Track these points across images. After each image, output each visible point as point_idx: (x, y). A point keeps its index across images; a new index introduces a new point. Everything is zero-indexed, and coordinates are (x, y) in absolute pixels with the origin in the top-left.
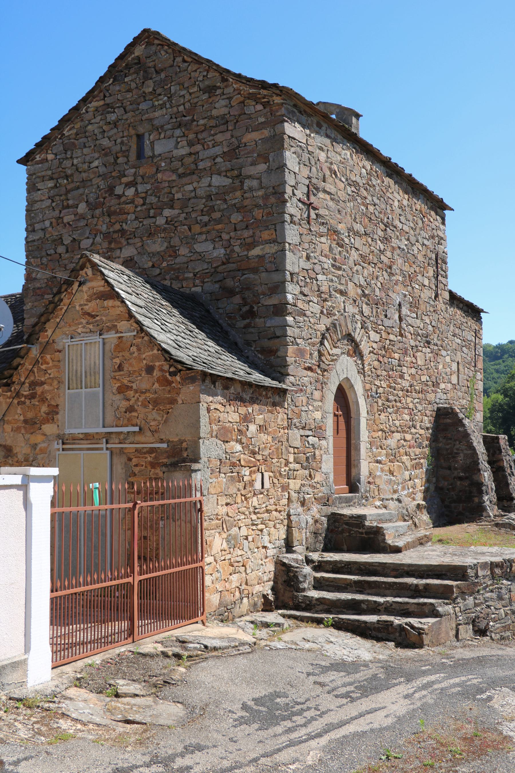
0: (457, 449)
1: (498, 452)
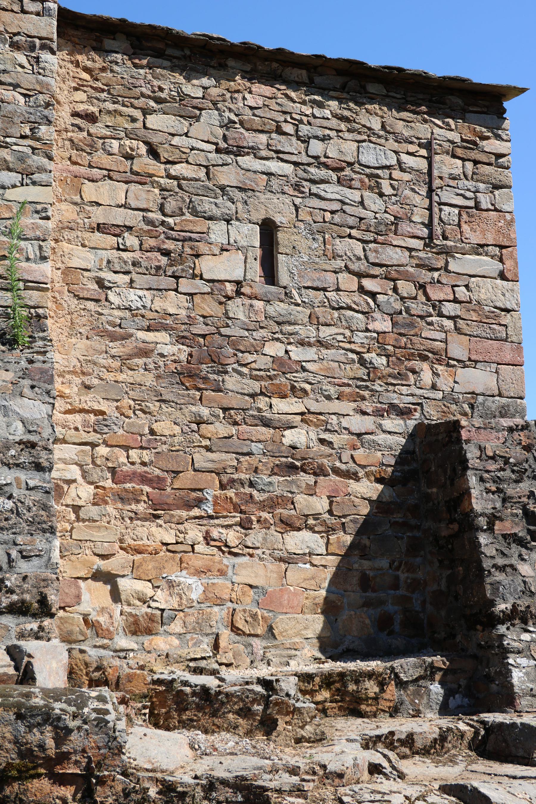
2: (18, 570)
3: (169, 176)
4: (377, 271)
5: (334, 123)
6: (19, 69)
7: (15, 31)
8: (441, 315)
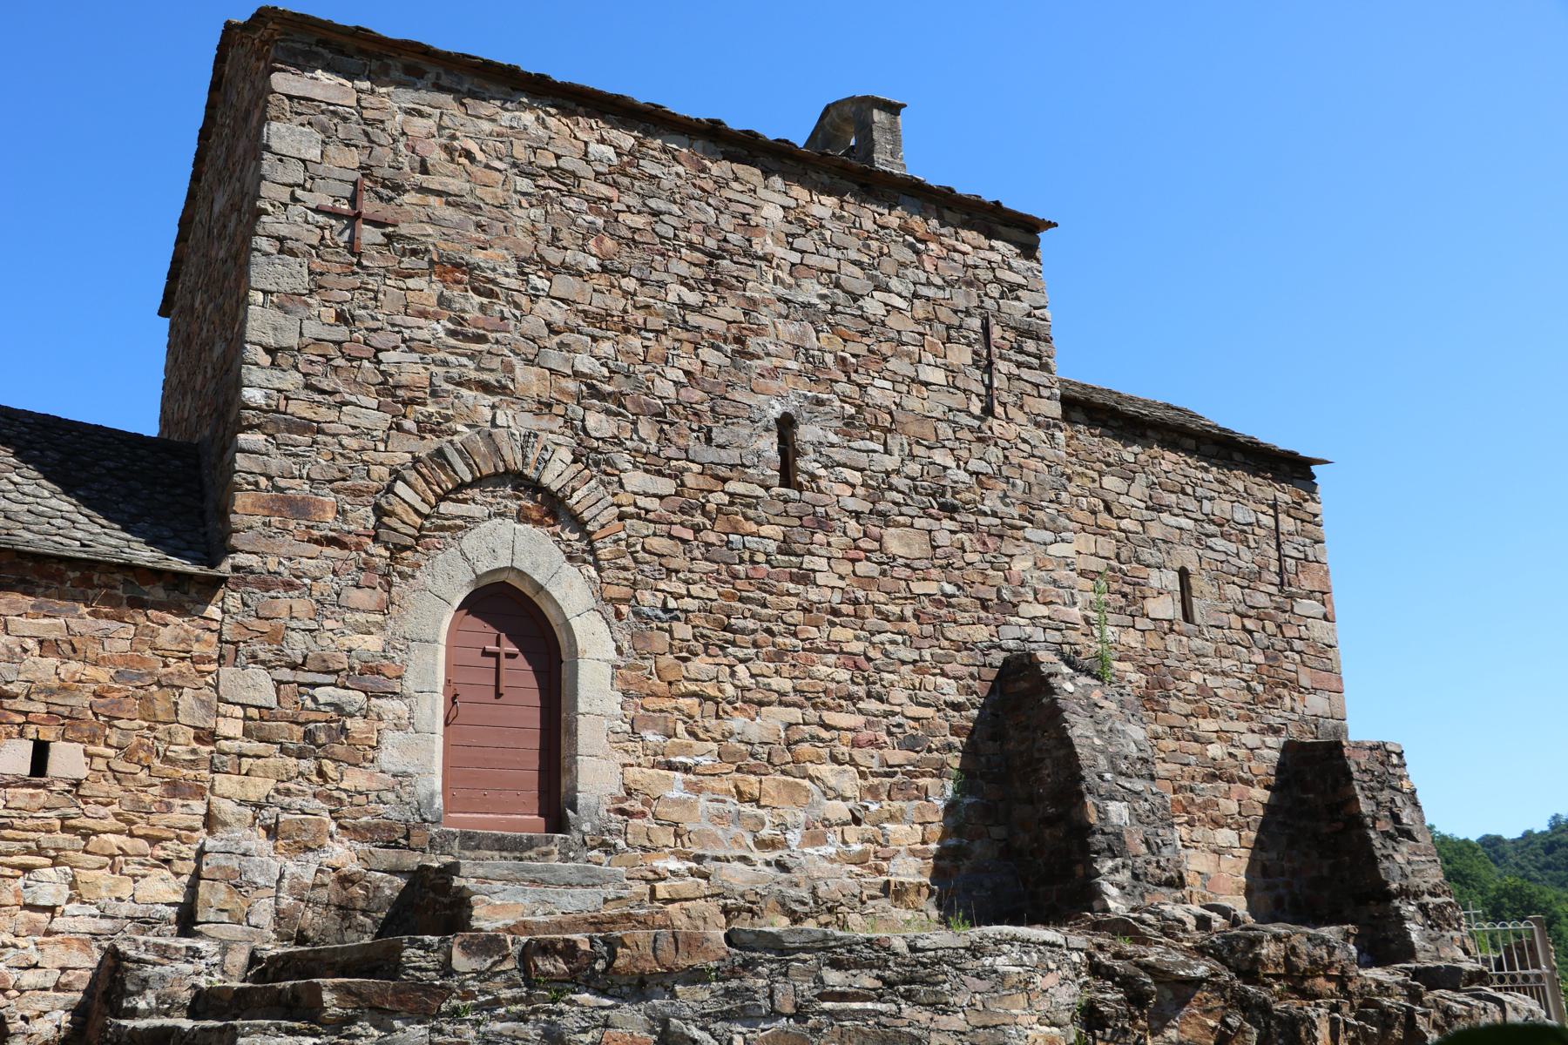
0: (1040, 750)
1: (1343, 780)
3: (1120, 530)
4: (1252, 612)
5: (1216, 486)
8: (1292, 650)
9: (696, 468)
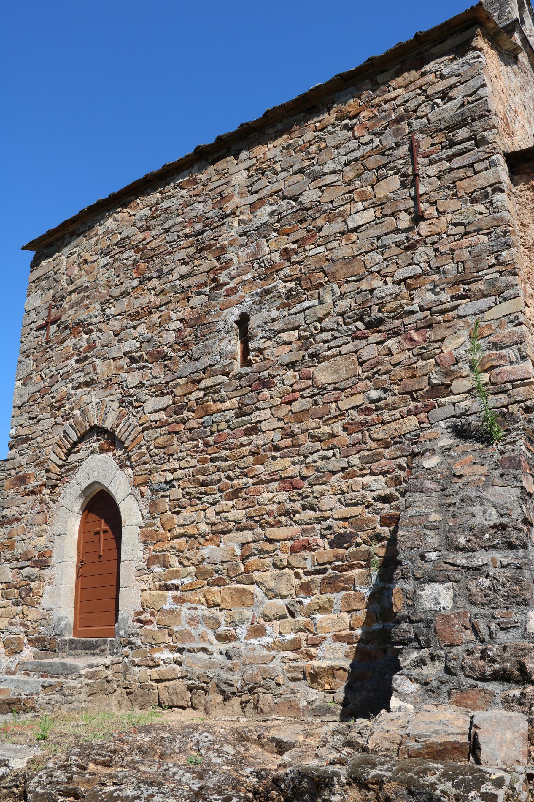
2: (498, 641)
6: (479, 216)
7: (472, 190)
9: (182, 381)
